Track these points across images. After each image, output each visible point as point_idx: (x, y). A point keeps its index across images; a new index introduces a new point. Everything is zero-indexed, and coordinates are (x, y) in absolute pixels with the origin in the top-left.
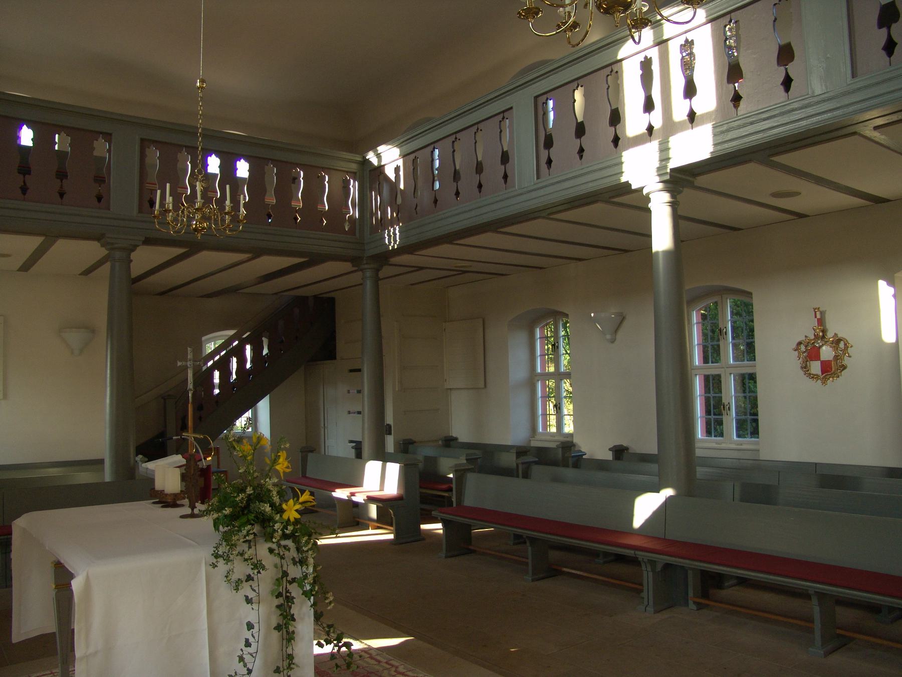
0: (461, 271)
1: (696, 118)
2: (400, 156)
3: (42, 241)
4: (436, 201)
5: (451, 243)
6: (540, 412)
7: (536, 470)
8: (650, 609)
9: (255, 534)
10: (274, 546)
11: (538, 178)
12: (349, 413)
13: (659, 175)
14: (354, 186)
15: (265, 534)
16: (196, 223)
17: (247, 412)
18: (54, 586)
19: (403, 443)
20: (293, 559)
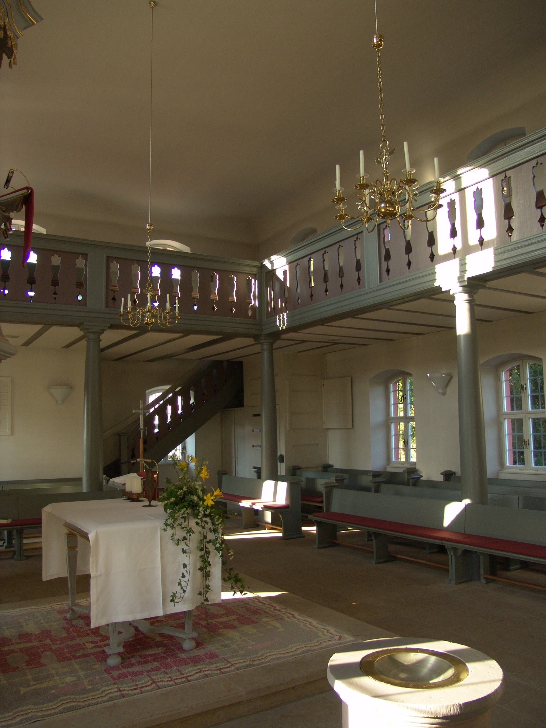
0: (334, 343)
1: (484, 243)
2: (286, 263)
3: (41, 327)
4: (312, 296)
5: (323, 325)
6: (393, 446)
7: (384, 487)
8: (453, 582)
9: (188, 514)
10: (199, 521)
11: (381, 282)
12: (253, 446)
13: (459, 282)
14: (255, 284)
15: (194, 514)
16: (148, 319)
17: (179, 446)
18: (67, 548)
19: (292, 469)
20: (210, 529)
